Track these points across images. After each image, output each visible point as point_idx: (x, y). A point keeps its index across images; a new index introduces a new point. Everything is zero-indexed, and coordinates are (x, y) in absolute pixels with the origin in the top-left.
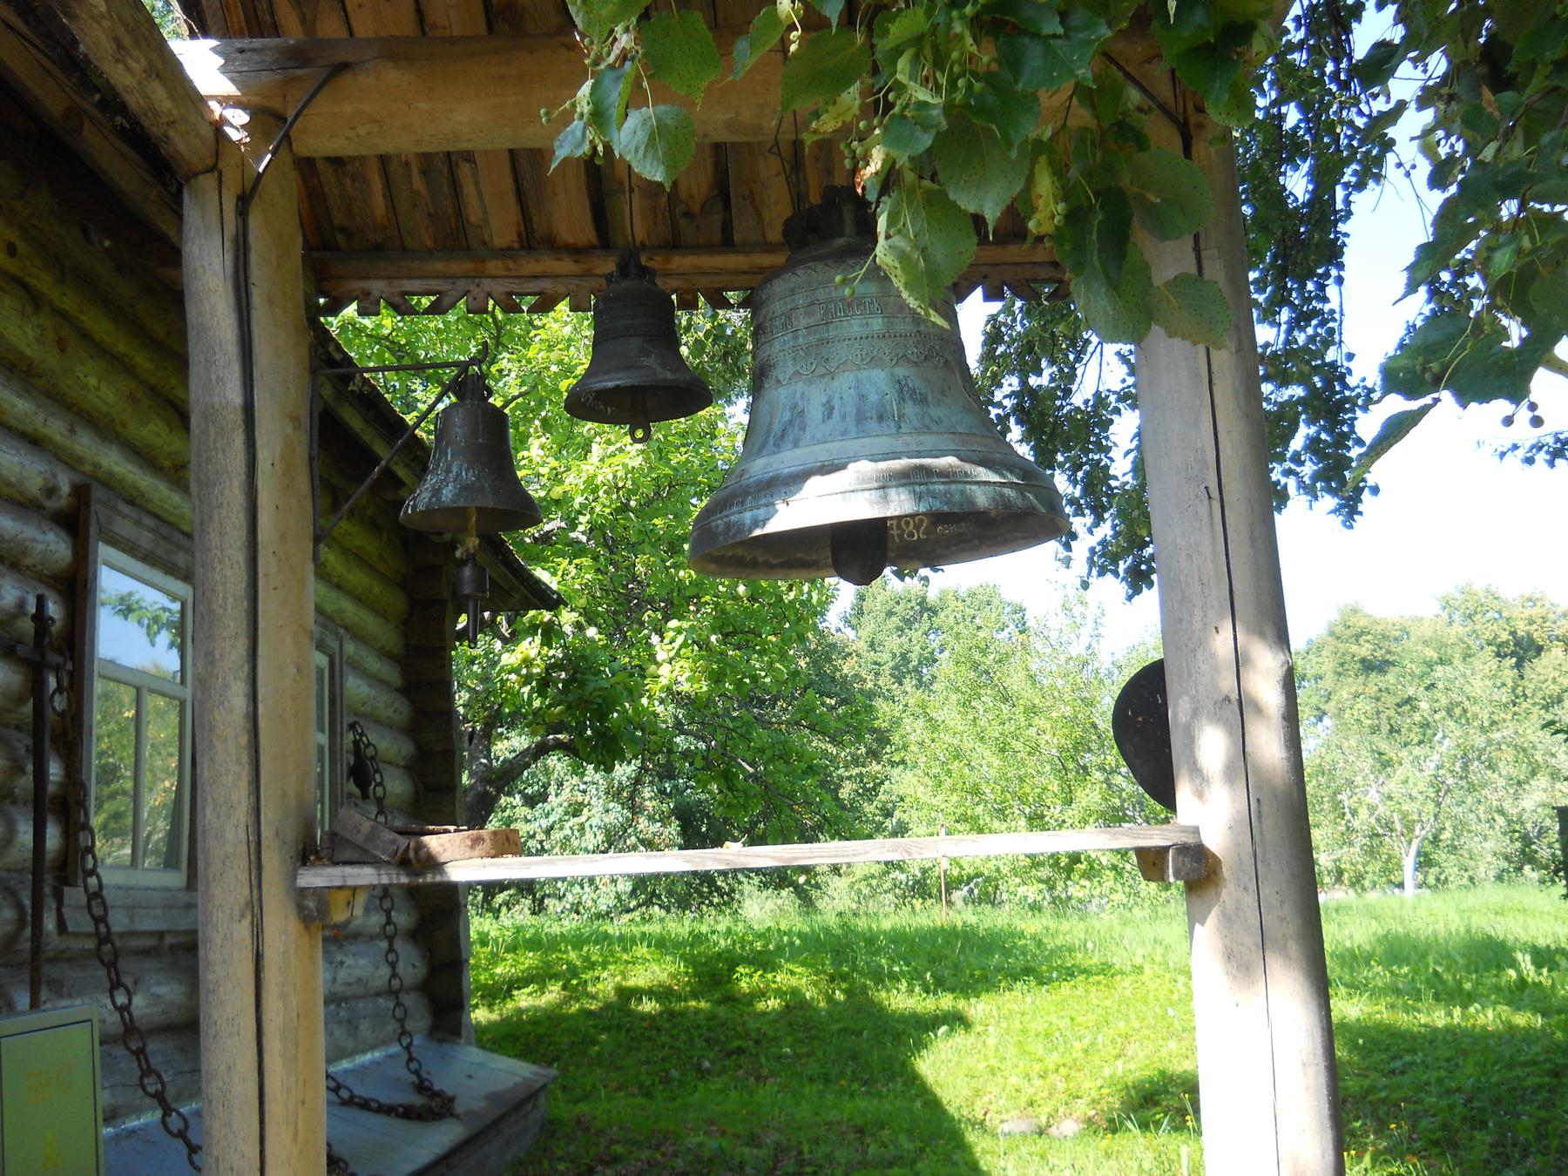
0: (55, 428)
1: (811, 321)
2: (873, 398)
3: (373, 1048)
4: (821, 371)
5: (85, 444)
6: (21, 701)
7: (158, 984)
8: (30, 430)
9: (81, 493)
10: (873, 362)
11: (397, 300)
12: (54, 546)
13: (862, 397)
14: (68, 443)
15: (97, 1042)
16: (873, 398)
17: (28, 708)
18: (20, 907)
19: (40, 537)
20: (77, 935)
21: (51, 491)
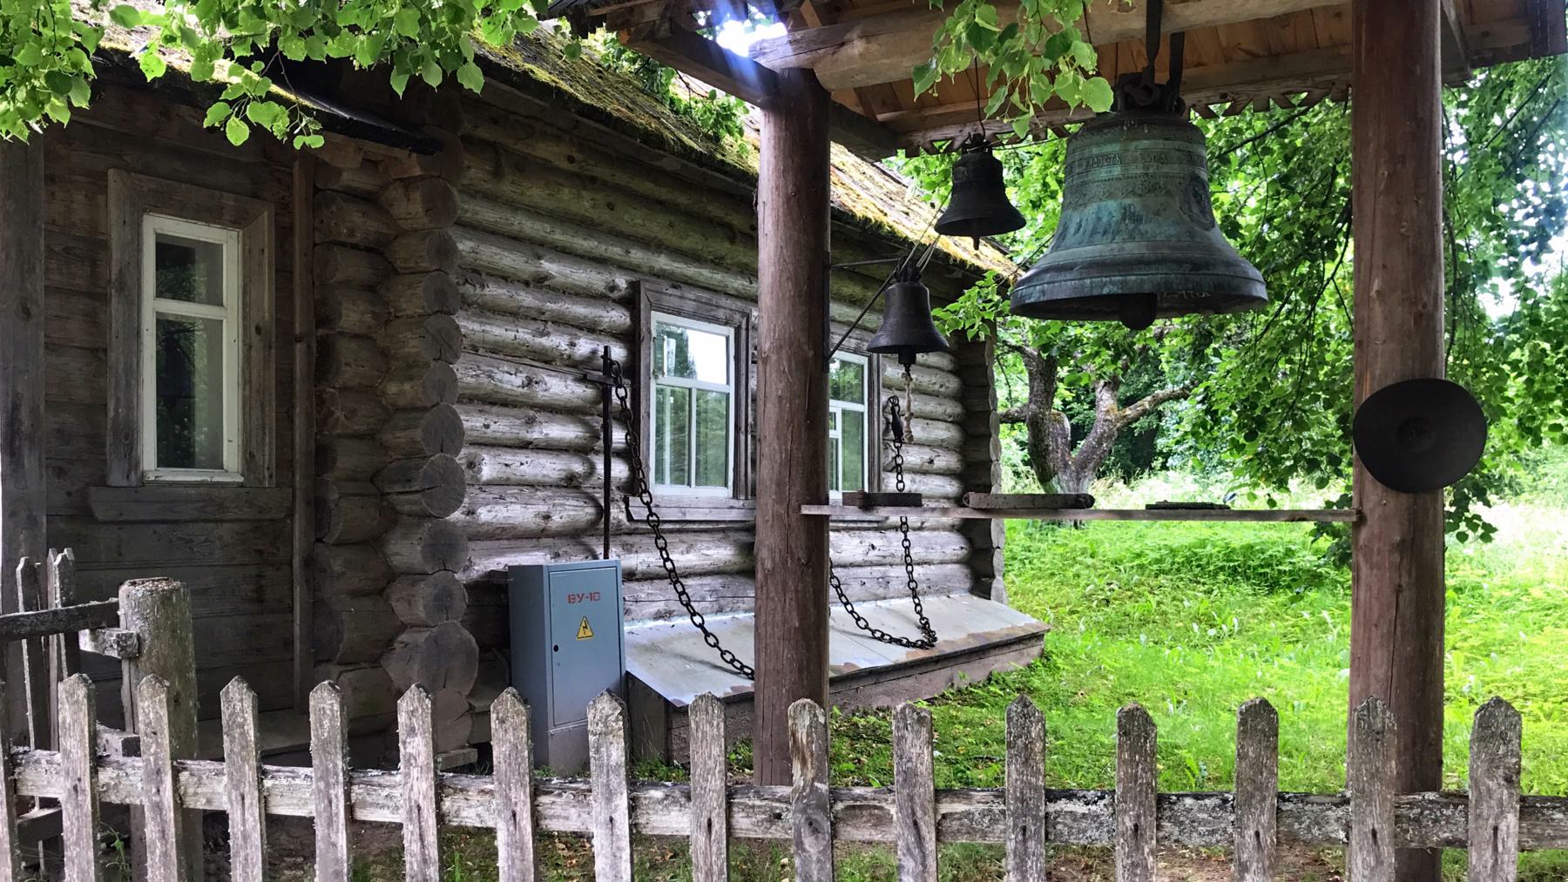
0: (615, 251)
1: (1081, 170)
2: (1105, 219)
3: (292, 590)
4: (1081, 202)
5: (637, 256)
6: (599, 403)
7: (708, 548)
8: (597, 255)
9: (634, 287)
10: (1110, 196)
11: (928, 146)
12: (617, 317)
13: (1099, 219)
14: (627, 259)
15: (620, 579)
16: (1105, 219)
17: (601, 406)
18: (597, 505)
19: (605, 314)
20: (638, 521)
21: (613, 288)
